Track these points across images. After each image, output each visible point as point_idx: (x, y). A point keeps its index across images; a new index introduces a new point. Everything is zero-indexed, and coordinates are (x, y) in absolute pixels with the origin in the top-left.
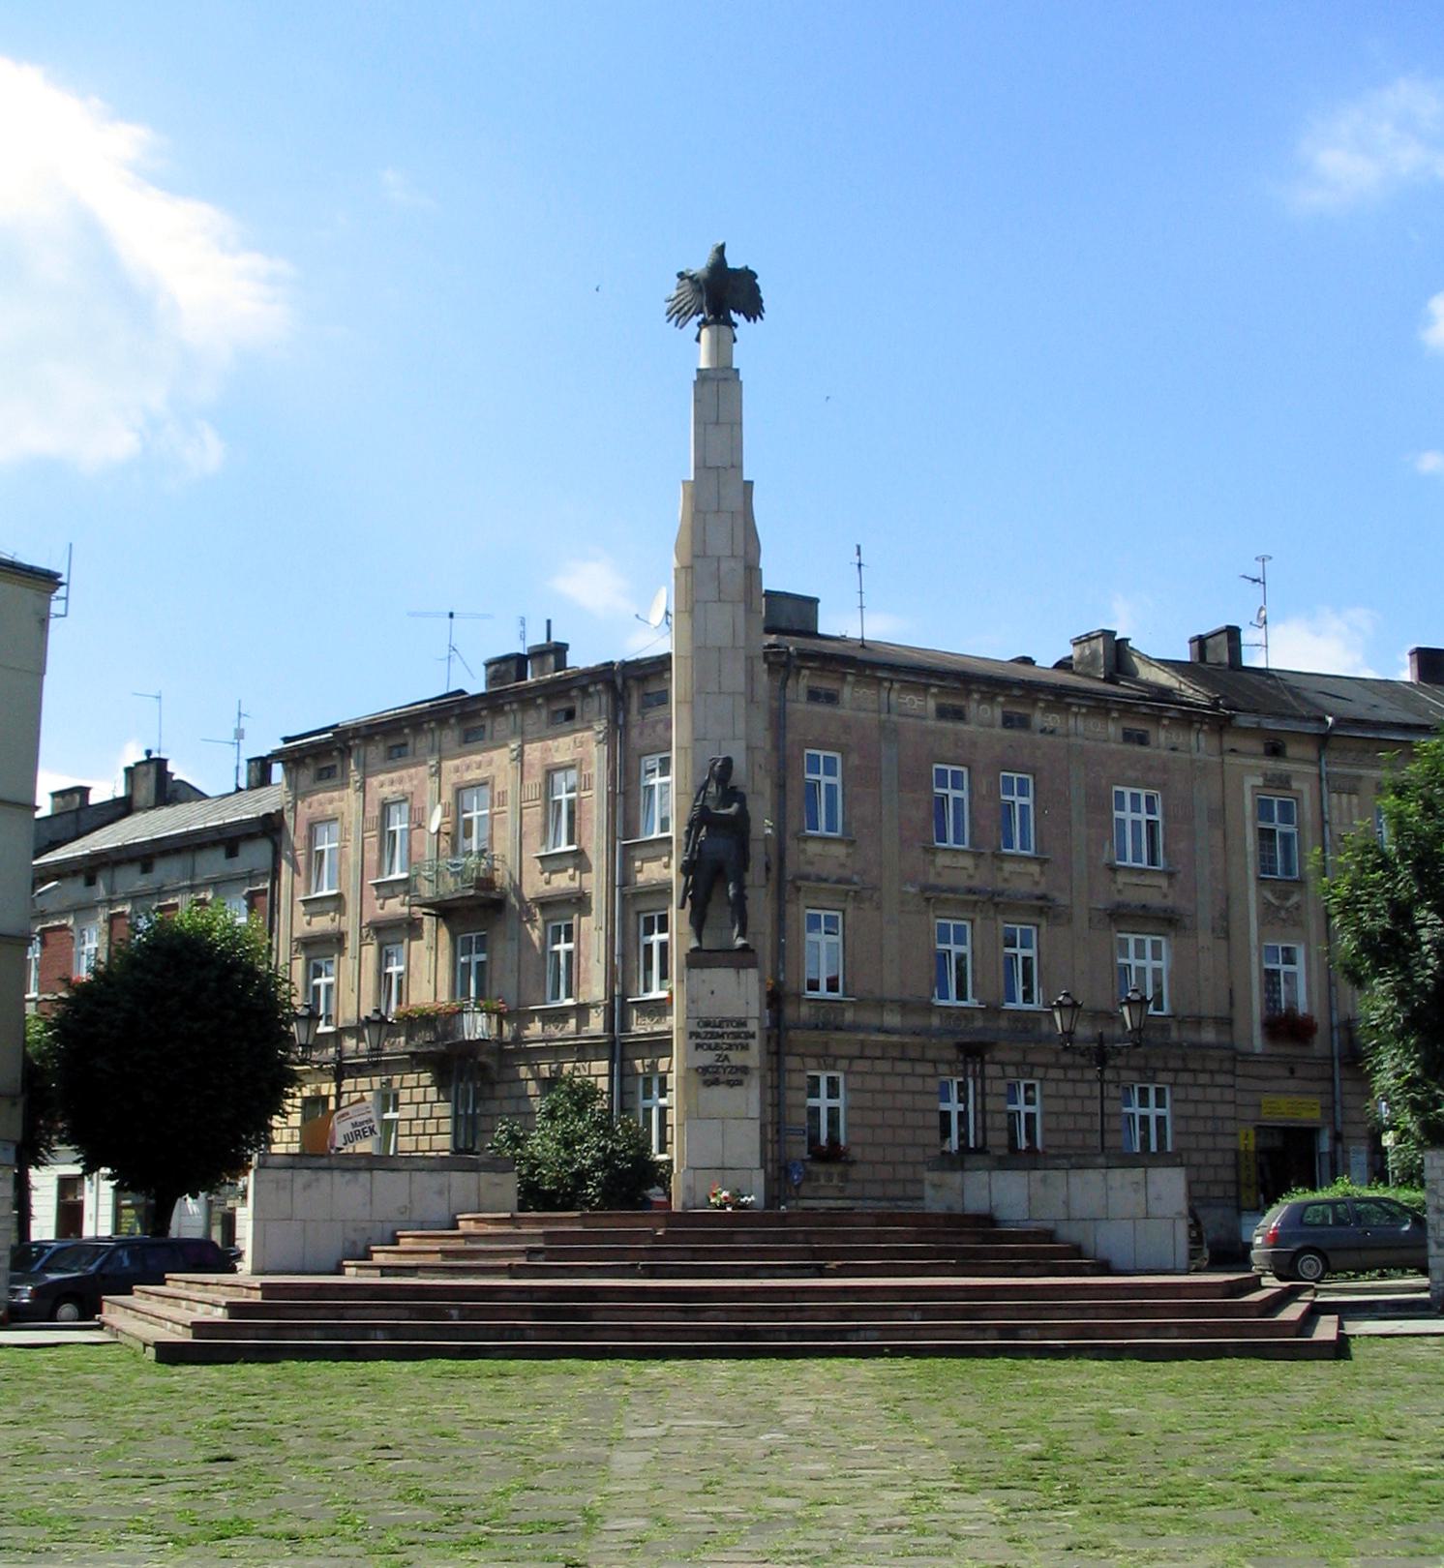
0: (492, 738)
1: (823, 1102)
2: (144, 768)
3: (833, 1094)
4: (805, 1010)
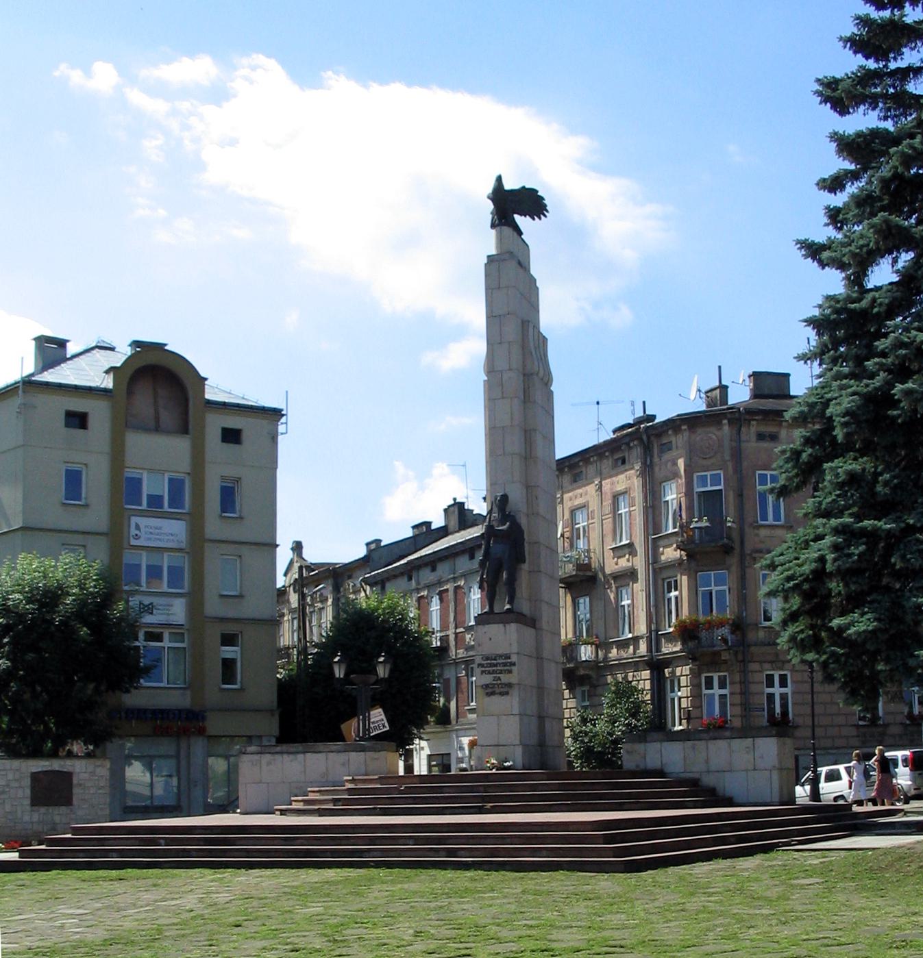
0: (586, 479)
1: (777, 690)
2: (452, 509)
3: (783, 683)
4: (761, 634)
